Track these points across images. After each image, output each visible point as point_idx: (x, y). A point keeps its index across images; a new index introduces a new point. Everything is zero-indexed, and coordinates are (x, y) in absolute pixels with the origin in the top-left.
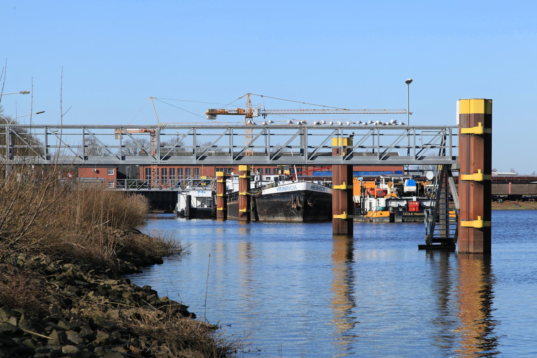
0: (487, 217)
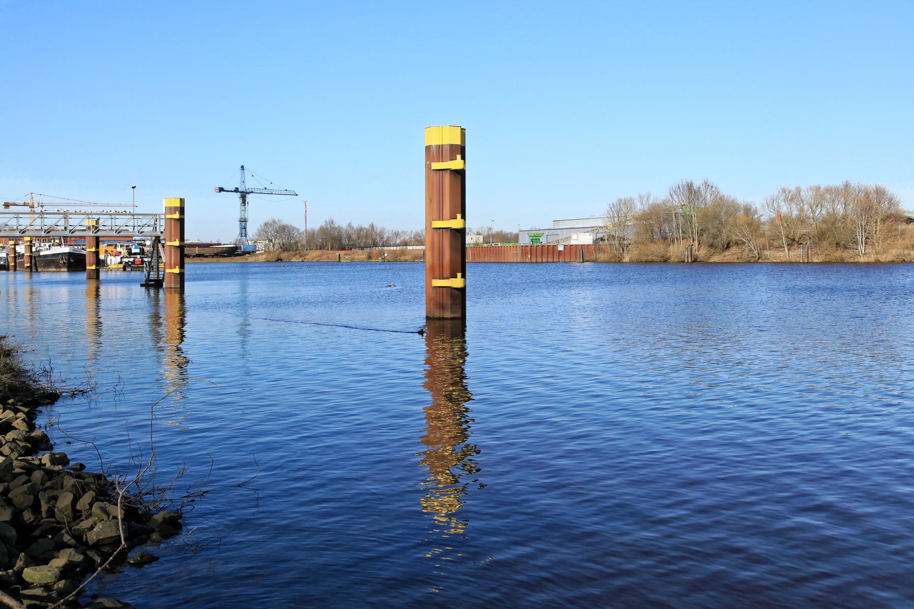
0: (182, 266)
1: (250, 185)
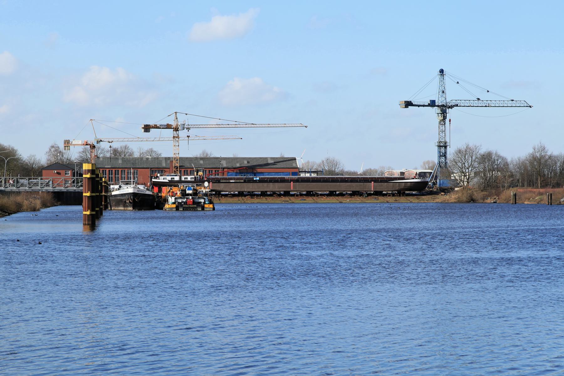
1: (450, 98)
